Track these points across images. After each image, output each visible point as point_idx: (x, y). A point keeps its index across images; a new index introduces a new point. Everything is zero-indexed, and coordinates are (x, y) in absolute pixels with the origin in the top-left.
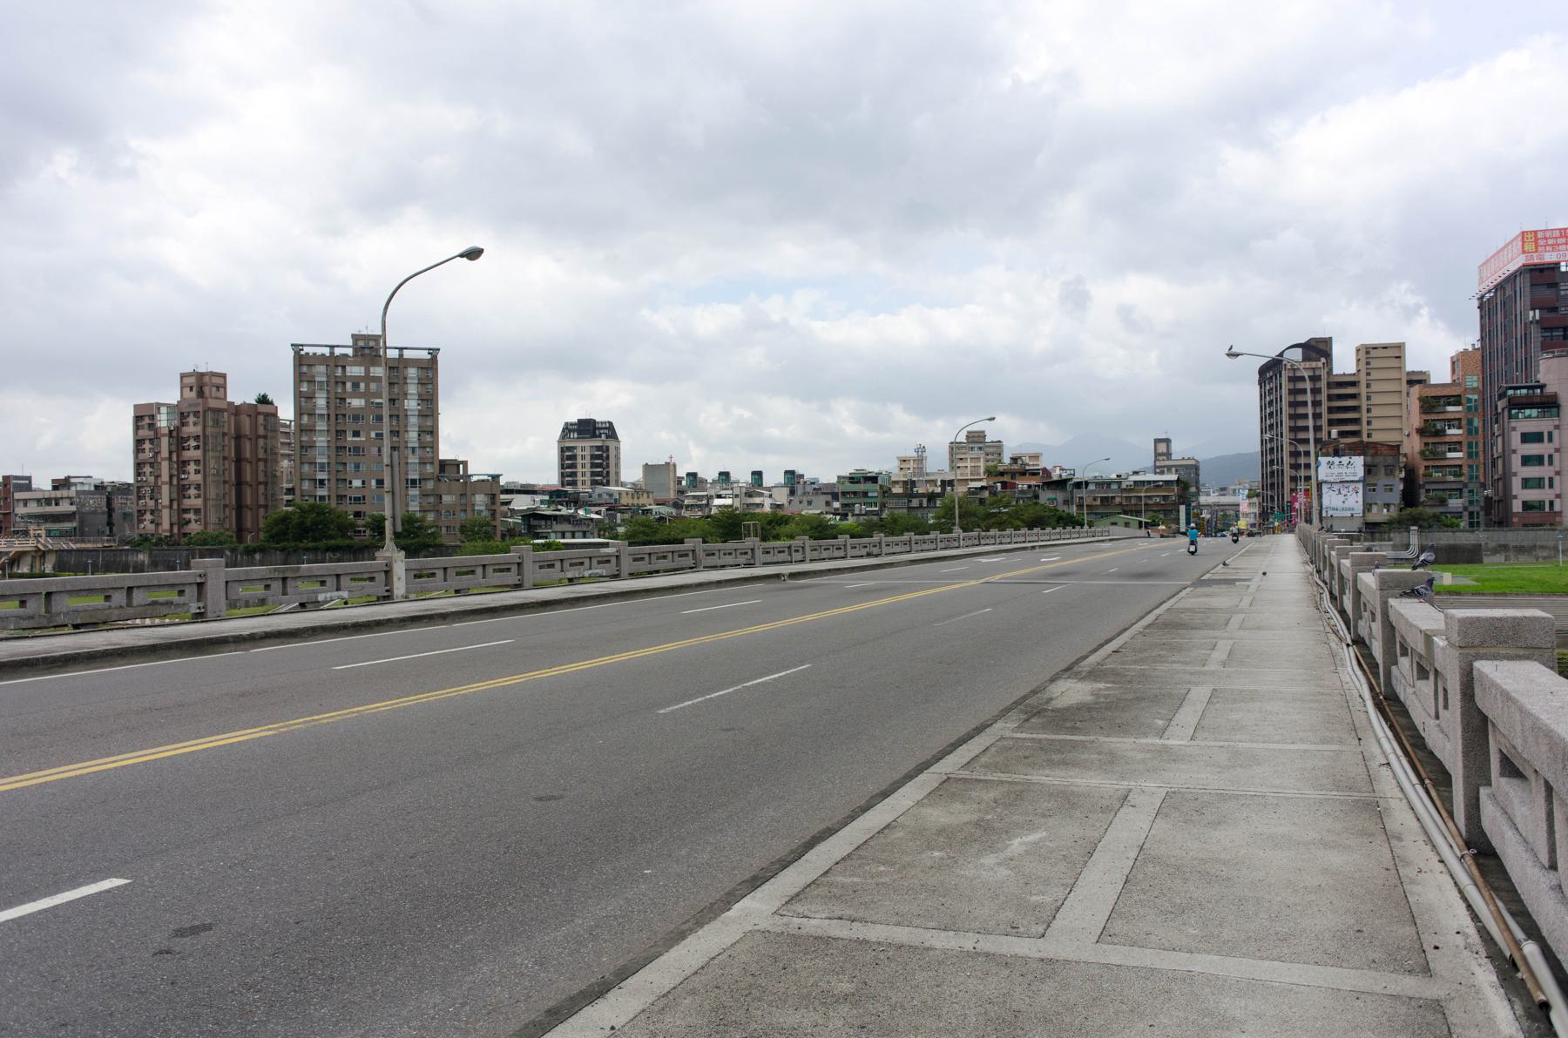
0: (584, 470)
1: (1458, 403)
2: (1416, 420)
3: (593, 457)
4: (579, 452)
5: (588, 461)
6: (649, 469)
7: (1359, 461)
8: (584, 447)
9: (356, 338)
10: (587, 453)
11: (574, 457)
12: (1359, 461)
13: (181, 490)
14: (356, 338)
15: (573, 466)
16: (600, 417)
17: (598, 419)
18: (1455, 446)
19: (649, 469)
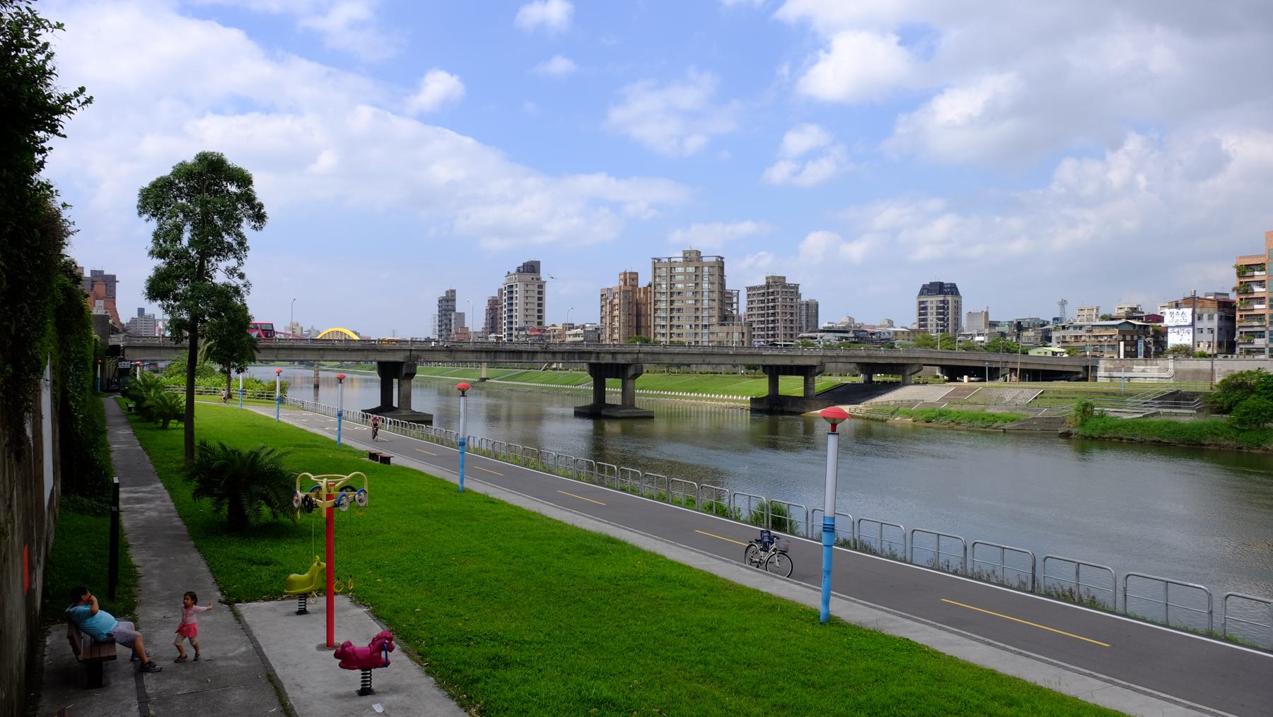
0: (932, 319)
1: (1263, 270)
2: (1235, 282)
3: (938, 308)
4: (929, 305)
5: (934, 310)
6: (92, 272)
7: (1189, 311)
8: (933, 301)
9: (685, 252)
10: (934, 305)
11: (925, 308)
12: (1189, 311)
13: (613, 318)
14: (685, 252)
15: (926, 314)
16: (946, 280)
17: (945, 282)
18: (1261, 300)
19: (92, 272)
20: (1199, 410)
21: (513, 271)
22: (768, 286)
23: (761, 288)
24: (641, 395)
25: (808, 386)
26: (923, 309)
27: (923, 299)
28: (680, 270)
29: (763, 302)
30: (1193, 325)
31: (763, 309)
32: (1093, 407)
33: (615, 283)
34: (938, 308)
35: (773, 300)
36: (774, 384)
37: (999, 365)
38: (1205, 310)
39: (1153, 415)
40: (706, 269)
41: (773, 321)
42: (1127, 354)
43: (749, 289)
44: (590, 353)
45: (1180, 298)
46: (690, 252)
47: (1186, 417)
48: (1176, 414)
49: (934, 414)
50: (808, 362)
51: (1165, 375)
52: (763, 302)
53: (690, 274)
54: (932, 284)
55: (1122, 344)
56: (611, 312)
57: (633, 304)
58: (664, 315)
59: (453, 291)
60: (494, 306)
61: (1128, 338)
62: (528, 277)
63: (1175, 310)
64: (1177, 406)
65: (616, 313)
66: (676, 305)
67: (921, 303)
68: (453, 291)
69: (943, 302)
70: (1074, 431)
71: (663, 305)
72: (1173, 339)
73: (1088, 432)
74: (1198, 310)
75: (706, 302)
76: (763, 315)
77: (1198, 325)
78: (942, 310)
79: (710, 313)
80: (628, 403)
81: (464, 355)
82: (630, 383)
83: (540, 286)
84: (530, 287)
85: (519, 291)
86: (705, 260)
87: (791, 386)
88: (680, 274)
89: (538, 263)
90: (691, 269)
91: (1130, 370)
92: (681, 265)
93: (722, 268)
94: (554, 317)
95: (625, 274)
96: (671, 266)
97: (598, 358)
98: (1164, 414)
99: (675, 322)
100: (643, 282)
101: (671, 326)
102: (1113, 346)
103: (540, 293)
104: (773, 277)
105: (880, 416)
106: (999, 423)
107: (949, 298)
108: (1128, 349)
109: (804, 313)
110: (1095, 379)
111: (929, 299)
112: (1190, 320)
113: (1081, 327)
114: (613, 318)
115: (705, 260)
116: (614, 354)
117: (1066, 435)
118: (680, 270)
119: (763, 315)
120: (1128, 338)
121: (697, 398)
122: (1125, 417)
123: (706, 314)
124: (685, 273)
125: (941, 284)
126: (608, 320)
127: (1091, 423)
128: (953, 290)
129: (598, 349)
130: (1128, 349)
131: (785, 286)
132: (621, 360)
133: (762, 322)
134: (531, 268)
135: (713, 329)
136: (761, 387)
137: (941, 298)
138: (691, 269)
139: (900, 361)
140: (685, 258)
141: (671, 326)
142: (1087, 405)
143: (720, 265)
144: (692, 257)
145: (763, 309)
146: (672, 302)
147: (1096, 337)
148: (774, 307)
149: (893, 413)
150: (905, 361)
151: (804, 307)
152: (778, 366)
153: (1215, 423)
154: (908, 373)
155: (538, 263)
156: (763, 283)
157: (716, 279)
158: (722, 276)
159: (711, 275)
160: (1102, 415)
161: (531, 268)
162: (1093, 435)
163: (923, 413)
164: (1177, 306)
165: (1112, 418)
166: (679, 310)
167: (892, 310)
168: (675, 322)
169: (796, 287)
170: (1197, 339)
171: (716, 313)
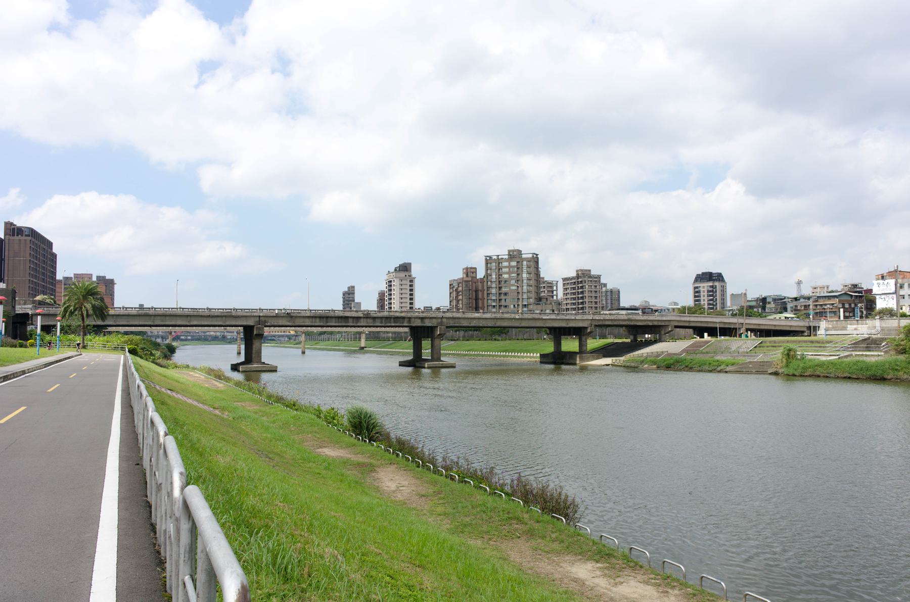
3: (708, 291)
4: (701, 289)
5: (706, 293)
7: (892, 282)
8: (705, 286)
9: (509, 251)
10: (706, 289)
12: (892, 282)
14: (509, 251)
15: (699, 296)
20: (886, 352)
21: (392, 270)
22: (578, 277)
23: (573, 278)
24: (446, 354)
25: (582, 345)
26: (697, 293)
27: (696, 285)
28: (506, 264)
29: (574, 288)
30: (895, 293)
31: (574, 294)
32: (795, 351)
33: (460, 275)
34: (708, 291)
35: (582, 287)
36: (558, 344)
37: (737, 326)
38: (905, 280)
39: (846, 357)
40: (525, 263)
41: (582, 303)
42: (845, 317)
43: (564, 280)
44: (403, 318)
45: (885, 272)
46: (513, 251)
47: (874, 357)
48: (866, 355)
49: (672, 361)
50: (581, 325)
51: (873, 331)
52: (574, 288)
53: (513, 267)
54: (703, 274)
55: (842, 310)
56: (457, 297)
57: (470, 290)
58: (494, 298)
59: (353, 287)
60: (382, 295)
61: (847, 306)
62: (402, 274)
63: (881, 281)
64: (868, 349)
65: (460, 297)
66: (504, 290)
67: (695, 288)
68: (353, 287)
69: (712, 287)
70: (780, 371)
71: (494, 291)
72: (880, 304)
73: (791, 371)
74: (900, 281)
75: (525, 288)
76: (574, 299)
77: (902, 292)
78: (712, 292)
79: (527, 296)
80: (435, 356)
81: (302, 320)
82: (437, 342)
83: (411, 281)
84: (404, 282)
85: (396, 284)
86: (524, 256)
87: (570, 345)
88: (506, 267)
89: (410, 264)
90: (514, 264)
91: (845, 328)
92: (506, 260)
93: (537, 262)
94: (420, 303)
95: (467, 269)
96: (499, 261)
97: (409, 322)
98: (856, 355)
99: (503, 303)
100: (481, 274)
101: (500, 306)
102: (835, 312)
103: (411, 286)
104: (581, 270)
105: (633, 364)
106: (722, 367)
107: (717, 284)
108: (847, 314)
109: (609, 297)
110: (816, 335)
111: (702, 285)
112: (893, 290)
113: (809, 298)
114: (458, 301)
115: (524, 256)
116: (422, 319)
117: (776, 374)
118: (506, 264)
119: (574, 299)
120: (847, 306)
121: (504, 356)
122: (824, 358)
123: (525, 296)
124: (509, 267)
125: (710, 274)
126: (454, 303)
127: (794, 363)
128: (719, 277)
129: (409, 315)
130: (847, 314)
131: (590, 277)
132: (428, 323)
133: (574, 304)
134: (405, 268)
135: (531, 307)
136: (549, 348)
137: (711, 284)
138: (514, 264)
139: (656, 323)
140: (509, 255)
141: (500, 306)
142: (790, 350)
143: (535, 260)
144: (515, 255)
145: (574, 294)
146: (500, 288)
147: (821, 305)
148: (582, 293)
149: (642, 362)
150: (660, 324)
151: (609, 294)
152: (560, 328)
153: (896, 361)
154: (663, 332)
155: (410, 264)
156: (574, 275)
157: (532, 269)
158: (537, 268)
159: (528, 267)
160: (803, 357)
161: (405, 268)
162: (797, 372)
163: (665, 361)
164: (883, 278)
165: (810, 360)
166: (505, 294)
167: (673, 294)
168: (503, 303)
169: (599, 277)
170: (901, 304)
171: (533, 295)
